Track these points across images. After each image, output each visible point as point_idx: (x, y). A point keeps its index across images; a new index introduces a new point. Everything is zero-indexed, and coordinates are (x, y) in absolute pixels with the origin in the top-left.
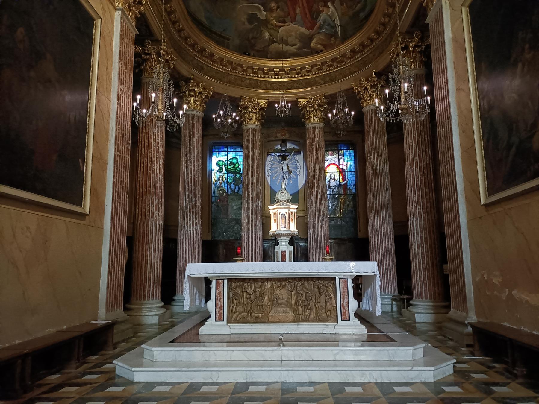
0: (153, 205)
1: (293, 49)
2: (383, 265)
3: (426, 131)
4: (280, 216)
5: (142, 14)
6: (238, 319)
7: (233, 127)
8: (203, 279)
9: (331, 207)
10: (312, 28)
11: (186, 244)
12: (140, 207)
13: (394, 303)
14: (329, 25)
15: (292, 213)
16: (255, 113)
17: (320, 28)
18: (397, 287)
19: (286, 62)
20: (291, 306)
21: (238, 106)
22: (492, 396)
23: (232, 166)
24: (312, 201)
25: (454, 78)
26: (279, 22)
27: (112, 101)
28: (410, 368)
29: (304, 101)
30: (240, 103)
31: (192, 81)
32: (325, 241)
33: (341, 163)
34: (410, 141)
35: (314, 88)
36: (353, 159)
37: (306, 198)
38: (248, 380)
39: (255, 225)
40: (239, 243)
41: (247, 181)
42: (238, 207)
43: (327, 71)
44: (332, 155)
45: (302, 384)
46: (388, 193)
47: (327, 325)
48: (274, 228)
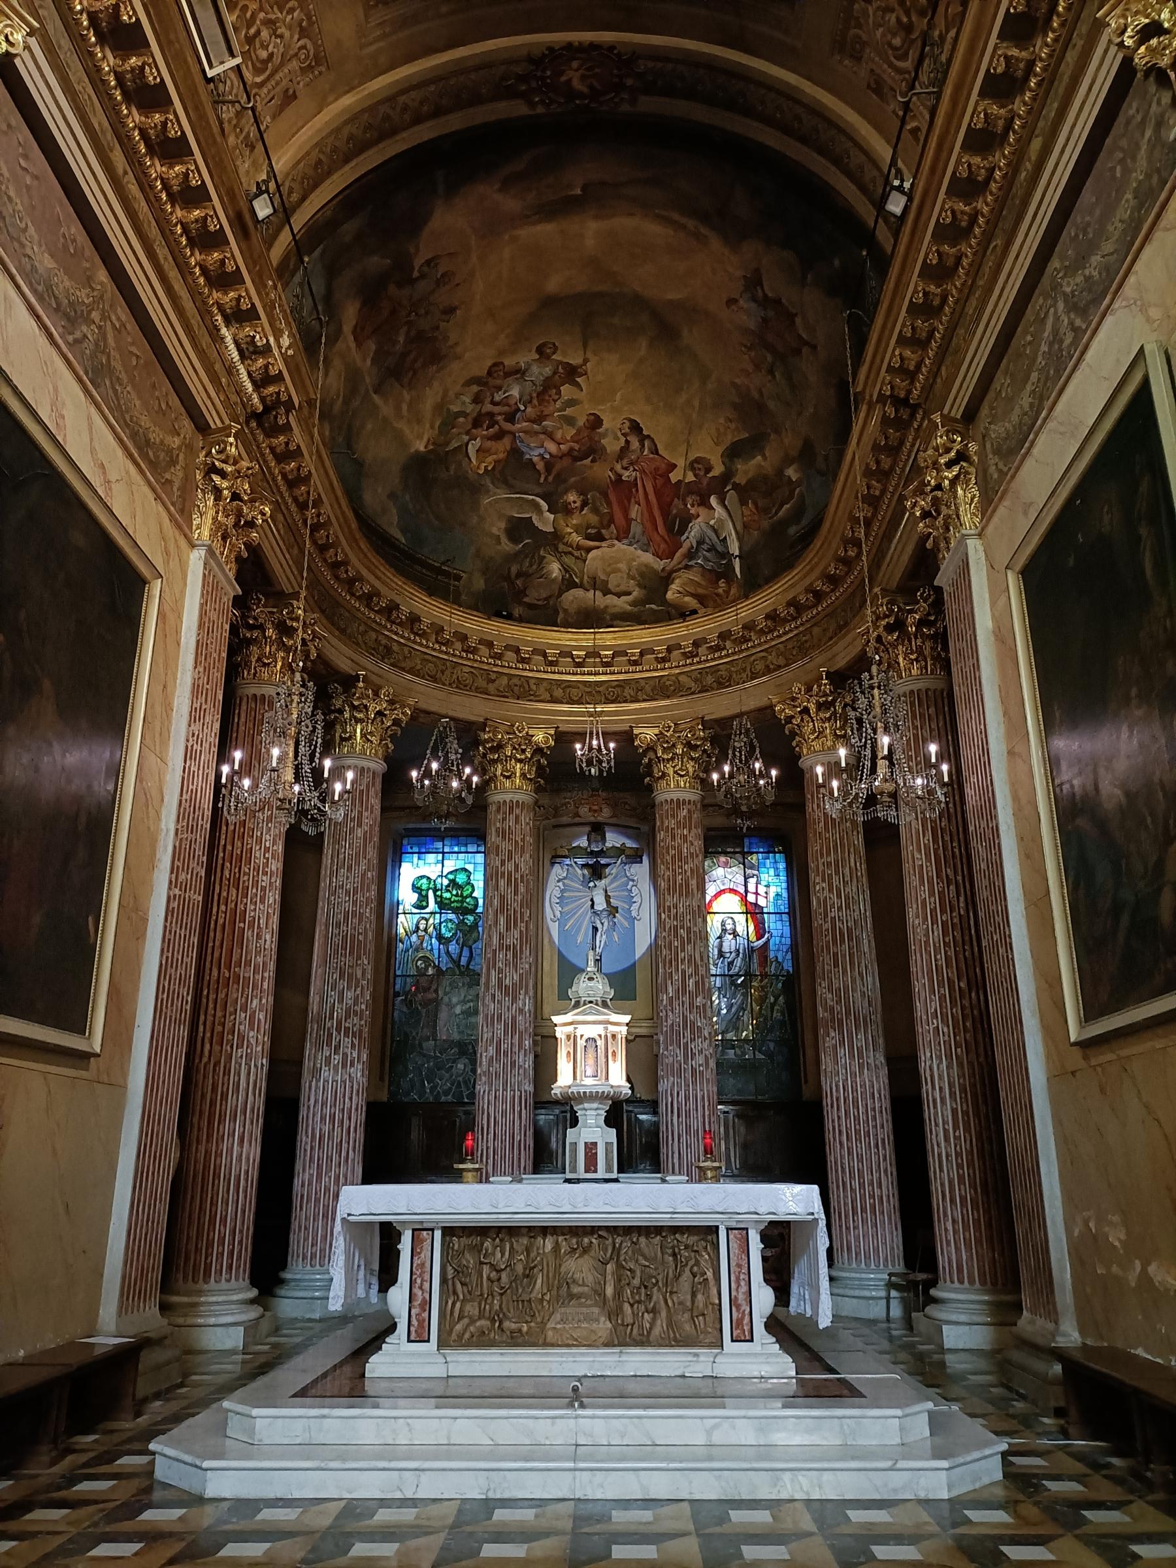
0: (243, 1015)
1: (621, 604)
2: (862, 1186)
3: (954, 830)
4: (581, 1043)
5: (254, 550)
6: (467, 1336)
7: (462, 800)
8: (377, 1228)
9: (724, 1011)
10: (671, 556)
11: (323, 1119)
12: (210, 1018)
13: (894, 1293)
14: (712, 549)
15: (614, 1036)
16: (520, 761)
17: (691, 555)
18: (901, 1248)
19: (604, 636)
20: (604, 1303)
21: (477, 743)
22: (1078, 1532)
23: (454, 892)
24: (671, 999)
25: (1002, 726)
26: (588, 537)
27: (170, 764)
28: (889, 1464)
29: (647, 734)
30: (482, 734)
31: (361, 684)
32: (707, 1113)
33: (751, 887)
34: (917, 855)
35: (675, 701)
36: (783, 878)
37: (656, 989)
38: (491, 1495)
39: (513, 1064)
40: (467, 1113)
41: (495, 940)
42: (467, 1006)
43: (707, 661)
44: (726, 865)
45: (626, 1504)
46: (872, 982)
47: (696, 1355)
48: (564, 1078)
